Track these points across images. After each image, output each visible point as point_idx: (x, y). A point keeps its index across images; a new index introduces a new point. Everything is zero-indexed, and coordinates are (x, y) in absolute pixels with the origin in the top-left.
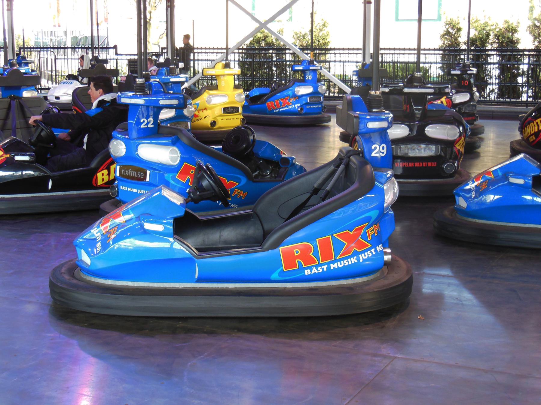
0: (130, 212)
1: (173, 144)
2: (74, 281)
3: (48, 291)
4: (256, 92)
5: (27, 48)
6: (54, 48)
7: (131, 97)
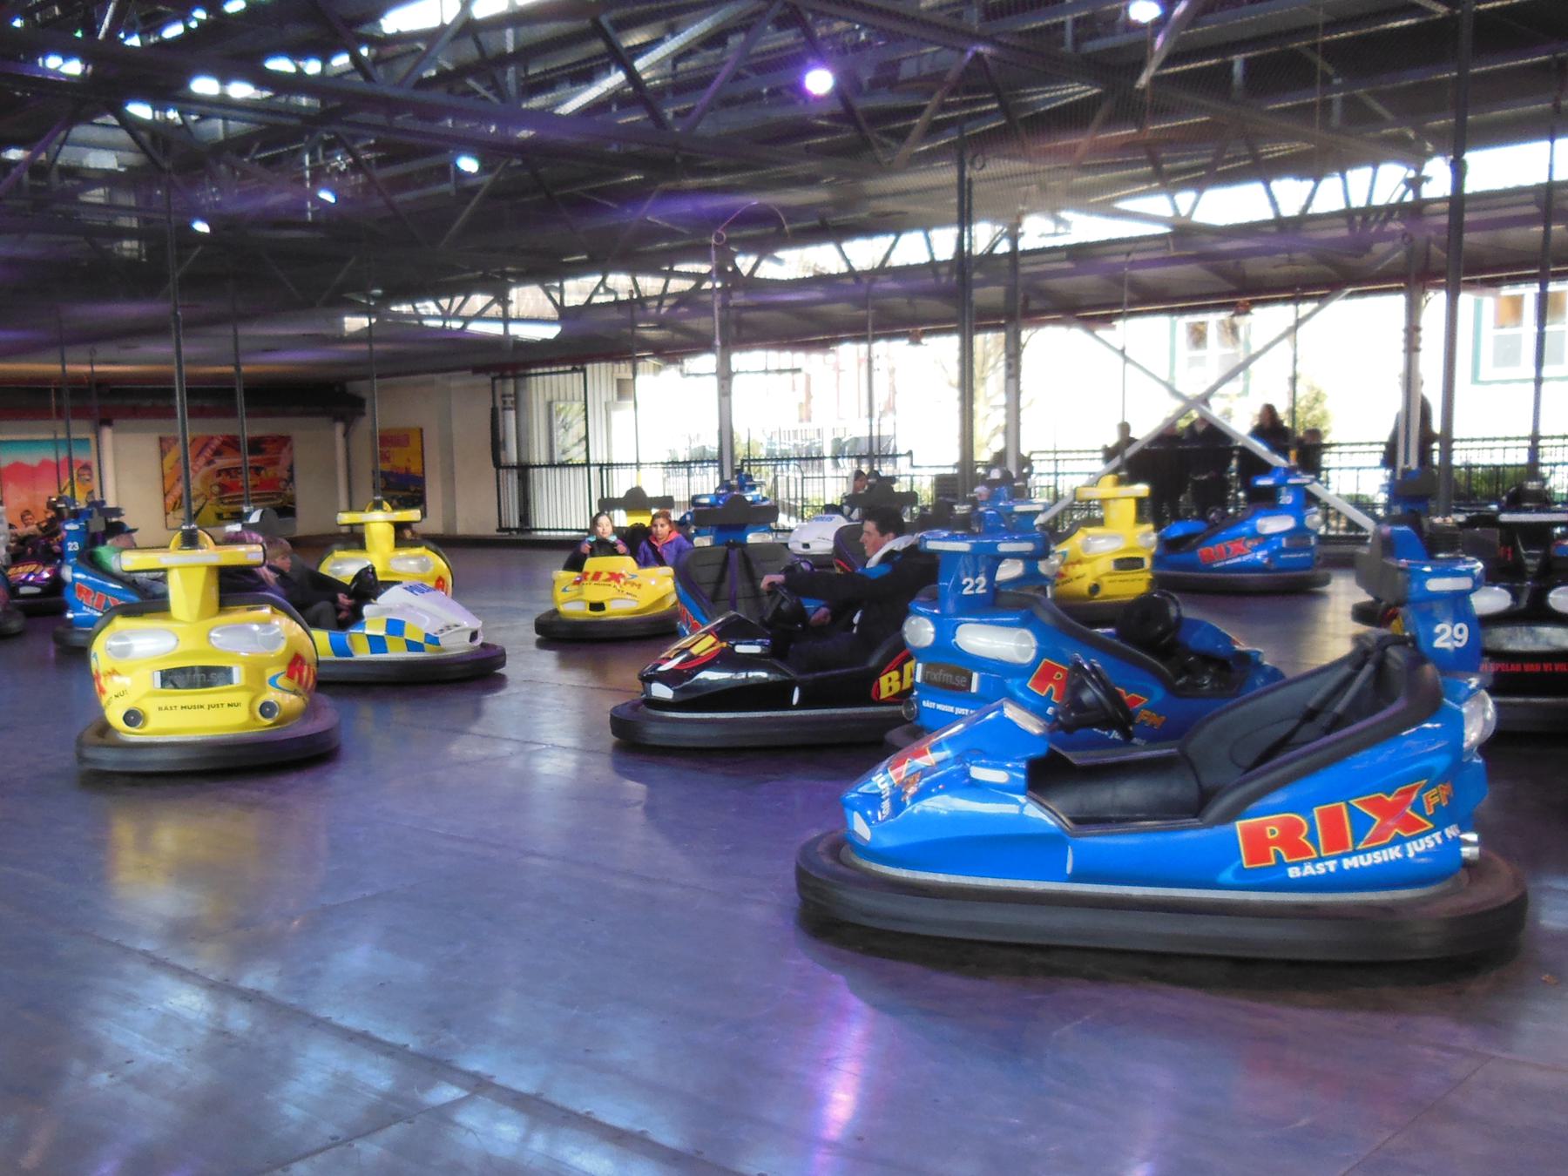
0: (944, 745)
1: (1023, 624)
2: (841, 869)
3: (793, 882)
4: (1177, 530)
5: (755, 460)
6: (800, 459)
7: (945, 539)
